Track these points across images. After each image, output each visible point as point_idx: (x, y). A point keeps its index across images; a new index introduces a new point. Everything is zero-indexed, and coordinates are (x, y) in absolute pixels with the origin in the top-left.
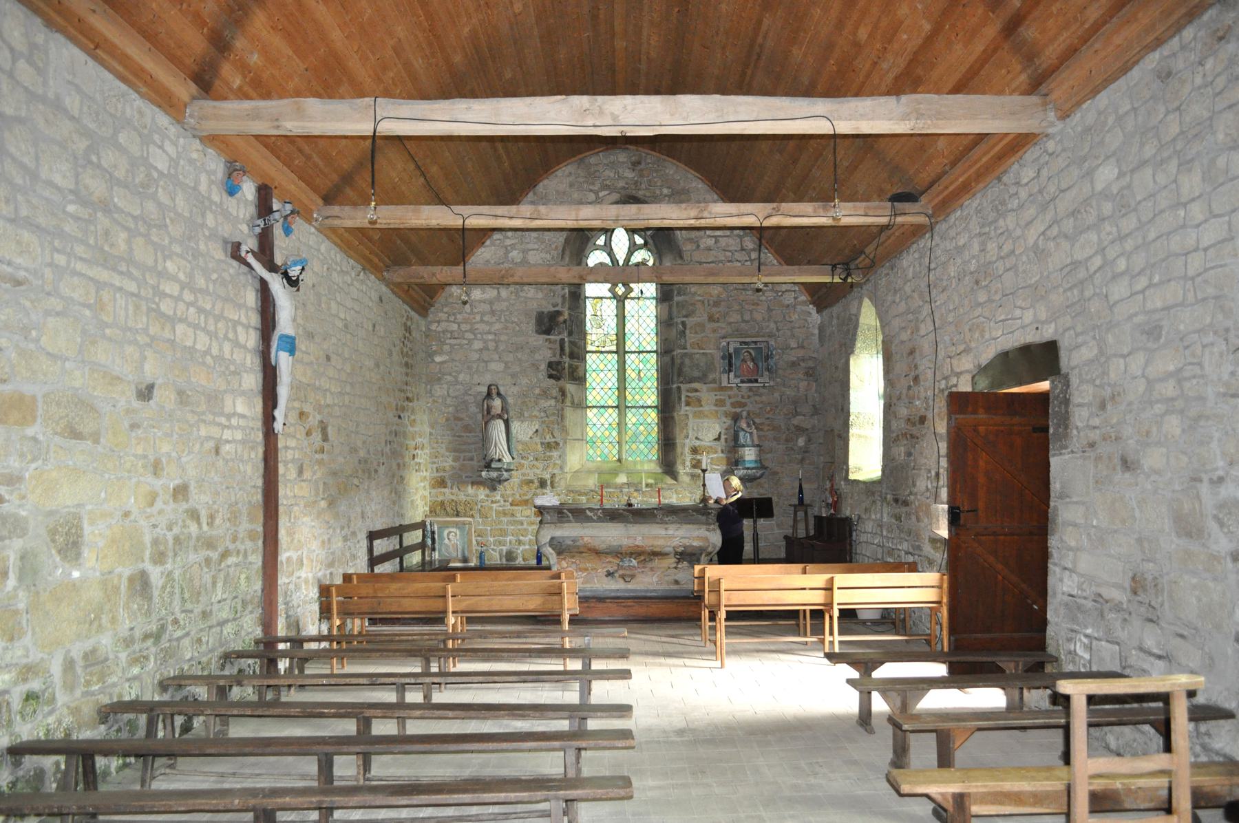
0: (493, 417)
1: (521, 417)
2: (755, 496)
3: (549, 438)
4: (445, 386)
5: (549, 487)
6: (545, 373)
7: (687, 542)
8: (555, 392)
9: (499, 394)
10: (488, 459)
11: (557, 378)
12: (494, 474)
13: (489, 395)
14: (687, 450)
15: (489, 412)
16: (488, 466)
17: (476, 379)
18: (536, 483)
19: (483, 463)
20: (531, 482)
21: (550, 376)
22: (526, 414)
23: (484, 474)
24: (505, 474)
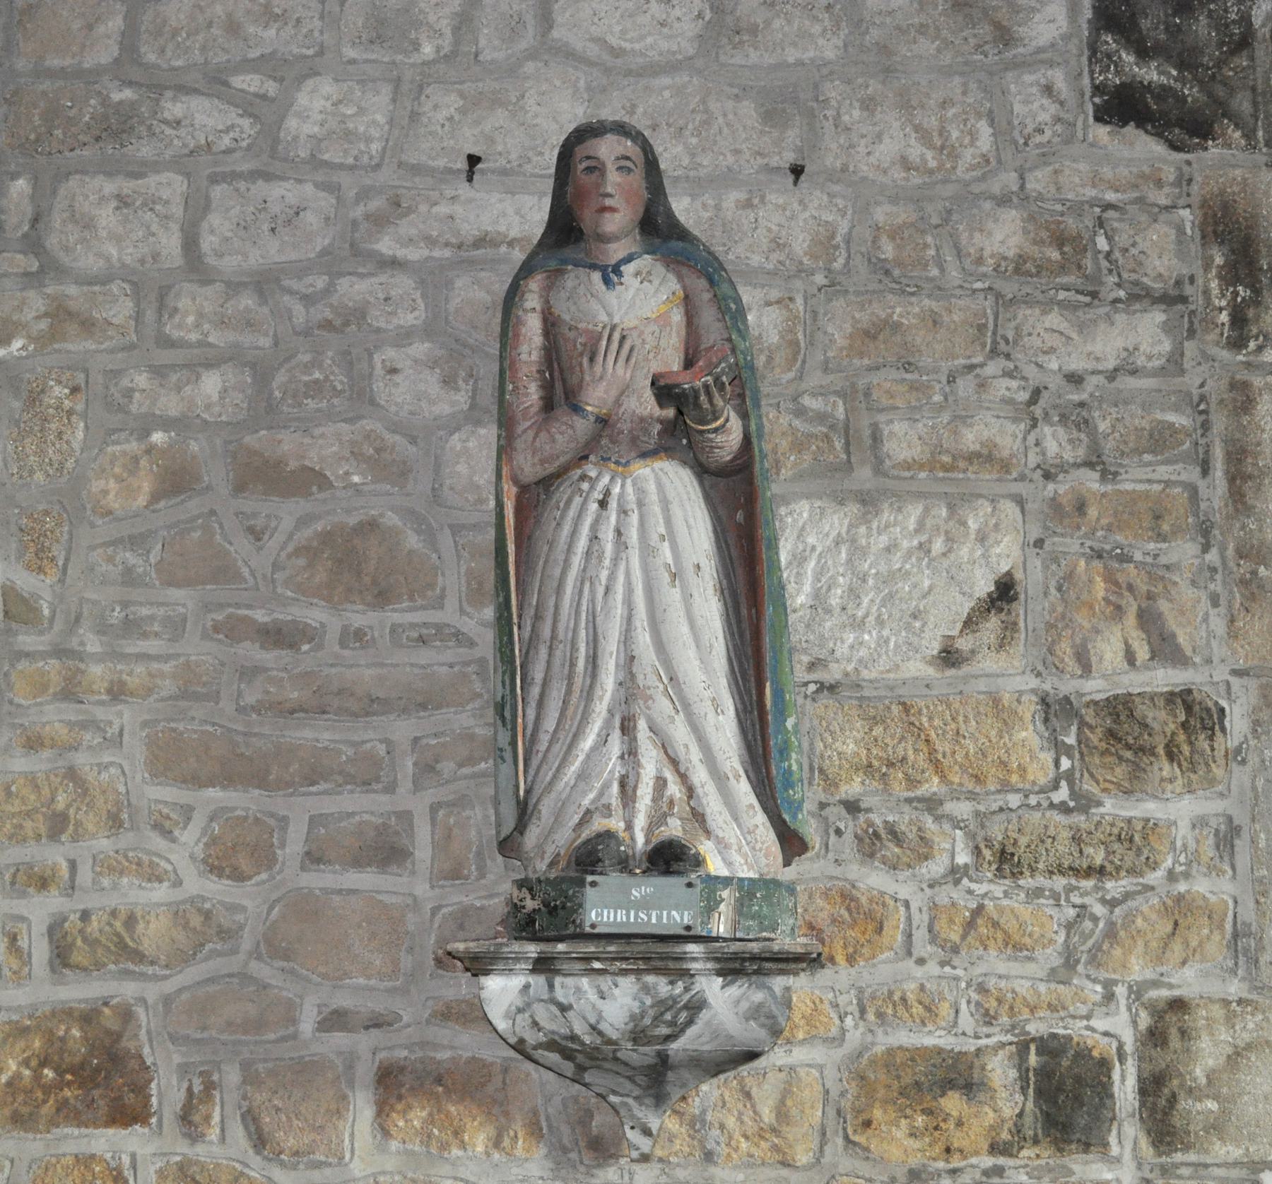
0: (607, 440)
1: (855, 467)
2: (792, 618)
3: (1114, 665)
4: (170, 187)
5: (1127, 1135)
6: (1069, 80)
7: (711, 591)
8: (1162, 251)
9: (658, 228)
10: (551, 840)
11: (1188, 127)
12: (610, 1003)
13: (567, 232)
14: (273, 544)
15: (560, 393)
16: (547, 921)
17: (447, 126)
18: (1006, 1096)
19: (496, 888)
20: (959, 1075)
21: (1122, 106)
22: (904, 440)
23: (501, 991)
24: (725, 1005)
